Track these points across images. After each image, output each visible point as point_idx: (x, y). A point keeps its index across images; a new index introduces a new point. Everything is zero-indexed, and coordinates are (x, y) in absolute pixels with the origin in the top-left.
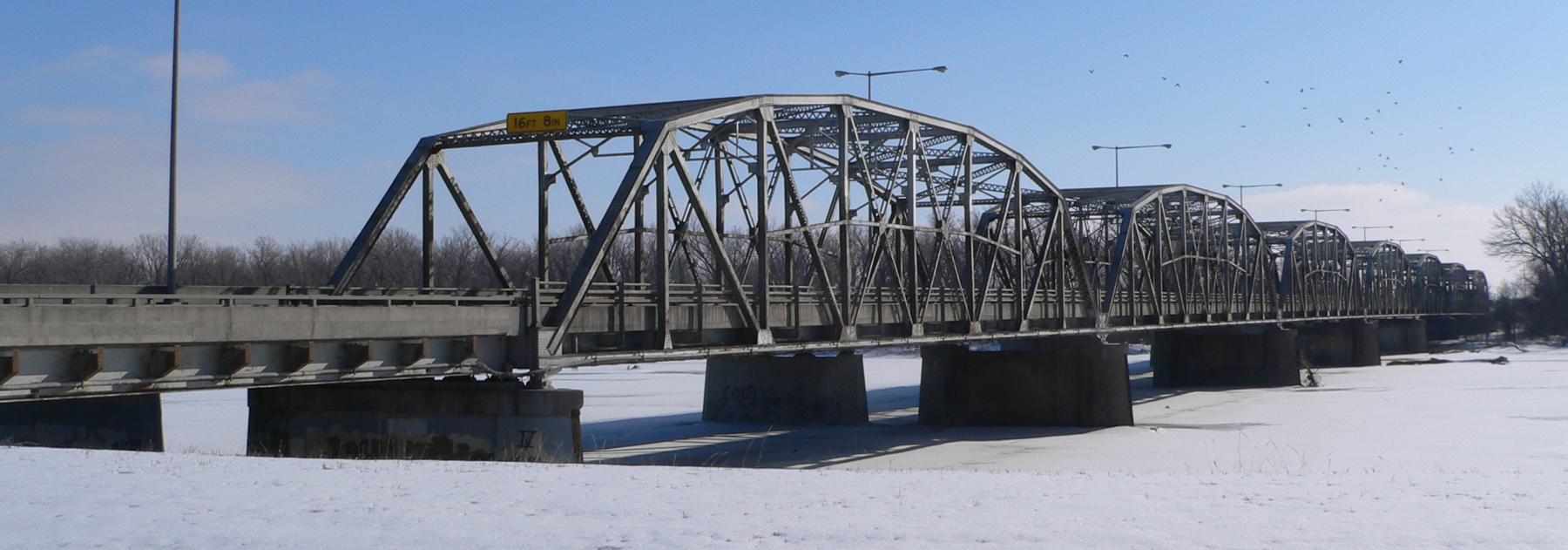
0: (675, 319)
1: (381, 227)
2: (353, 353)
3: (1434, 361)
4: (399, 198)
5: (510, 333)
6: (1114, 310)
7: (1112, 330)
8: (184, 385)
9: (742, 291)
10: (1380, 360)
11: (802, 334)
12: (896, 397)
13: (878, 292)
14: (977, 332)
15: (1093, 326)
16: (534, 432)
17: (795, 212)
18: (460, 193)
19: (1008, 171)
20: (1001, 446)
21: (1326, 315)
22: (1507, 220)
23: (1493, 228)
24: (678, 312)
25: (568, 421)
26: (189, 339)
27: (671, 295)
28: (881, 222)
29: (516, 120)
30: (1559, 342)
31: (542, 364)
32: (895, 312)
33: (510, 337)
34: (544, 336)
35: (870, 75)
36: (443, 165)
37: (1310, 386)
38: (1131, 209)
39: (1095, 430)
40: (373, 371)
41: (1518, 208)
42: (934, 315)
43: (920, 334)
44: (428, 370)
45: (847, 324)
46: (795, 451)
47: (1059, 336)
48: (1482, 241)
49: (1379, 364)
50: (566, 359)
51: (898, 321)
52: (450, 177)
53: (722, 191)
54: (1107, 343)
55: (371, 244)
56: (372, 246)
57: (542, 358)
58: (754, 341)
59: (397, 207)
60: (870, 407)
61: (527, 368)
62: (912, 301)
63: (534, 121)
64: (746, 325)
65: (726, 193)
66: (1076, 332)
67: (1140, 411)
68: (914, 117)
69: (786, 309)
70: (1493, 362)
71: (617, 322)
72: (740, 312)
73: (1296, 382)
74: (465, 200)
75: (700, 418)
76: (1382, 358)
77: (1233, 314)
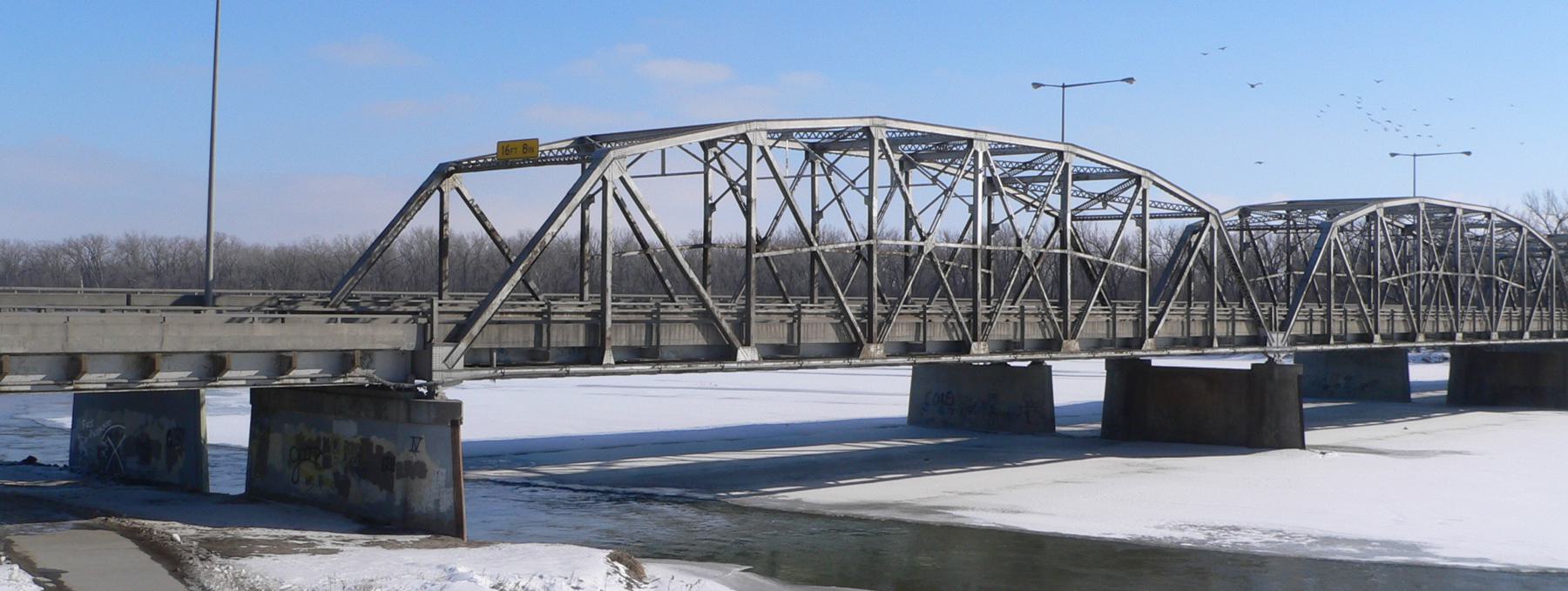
0: (1220, 330)
1: (386, 244)
2: (346, 361)
4: (408, 218)
6: (1297, 328)
7: (1294, 348)
8: (29, 388)
9: (716, 310)
11: (1349, 338)
12: (1078, 412)
13: (1222, 300)
16: (421, 439)
17: (914, 227)
24: (630, 330)
25: (447, 430)
27: (440, 313)
28: (926, 241)
31: (436, 377)
32: (1043, 325)
34: (439, 352)
35: (1064, 86)
40: (247, 380)
43: (982, 352)
44: (312, 379)
47: (1371, 349)
50: (469, 372)
51: (1048, 337)
55: (374, 260)
56: (375, 262)
61: (424, 380)
62: (1416, 309)
63: (516, 149)
66: (956, 359)
67: (1311, 437)
68: (979, 136)
69: (644, 331)
71: (545, 338)
75: (905, 422)
77: (1557, 332)
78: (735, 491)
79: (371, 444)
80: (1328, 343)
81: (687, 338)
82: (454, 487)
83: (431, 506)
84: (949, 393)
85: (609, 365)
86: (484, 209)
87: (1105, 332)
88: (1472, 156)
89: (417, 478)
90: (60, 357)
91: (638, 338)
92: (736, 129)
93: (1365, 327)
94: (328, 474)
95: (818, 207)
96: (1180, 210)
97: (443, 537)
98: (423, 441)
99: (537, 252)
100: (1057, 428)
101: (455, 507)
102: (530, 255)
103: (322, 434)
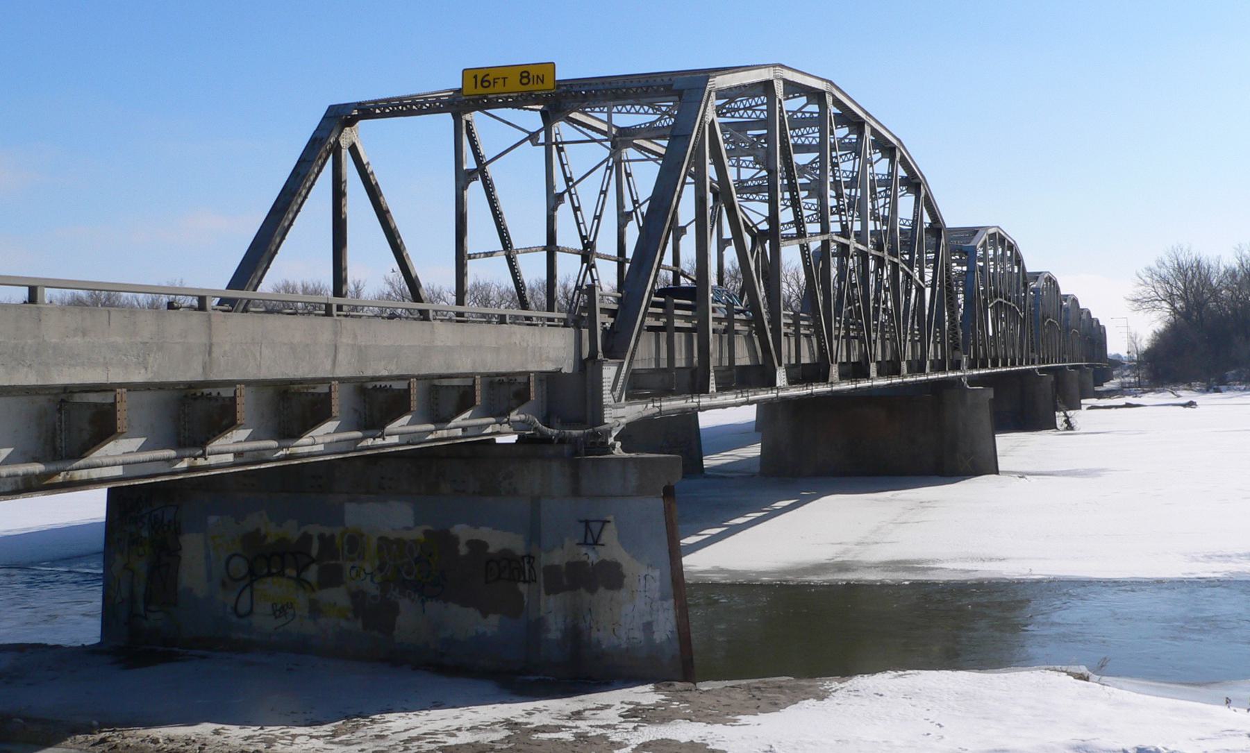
3: (1128, 405)
10: (1081, 404)
16: (605, 522)
18: (377, 184)
21: (897, 372)
22: (1148, 280)
23: (1135, 287)
26: (138, 377)
29: (476, 77)
30: (1204, 389)
36: (357, 145)
37: (1067, 429)
39: (964, 479)
41: (1157, 269)
48: (1124, 298)
49: (1080, 408)
52: (365, 163)
53: (624, 207)
54: (968, 387)
59: (305, 197)
70: (1184, 405)
73: (1051, 425)
74: (381, 195)
76: (1083, 401)
79: (455, 540)
80: (867, 376)
83: (638, 635)
89: (601, 590)
90: (147, 396)
93: (1003, 352)
94: (337, 596)
101: (678, 630)
103: (314, 530)
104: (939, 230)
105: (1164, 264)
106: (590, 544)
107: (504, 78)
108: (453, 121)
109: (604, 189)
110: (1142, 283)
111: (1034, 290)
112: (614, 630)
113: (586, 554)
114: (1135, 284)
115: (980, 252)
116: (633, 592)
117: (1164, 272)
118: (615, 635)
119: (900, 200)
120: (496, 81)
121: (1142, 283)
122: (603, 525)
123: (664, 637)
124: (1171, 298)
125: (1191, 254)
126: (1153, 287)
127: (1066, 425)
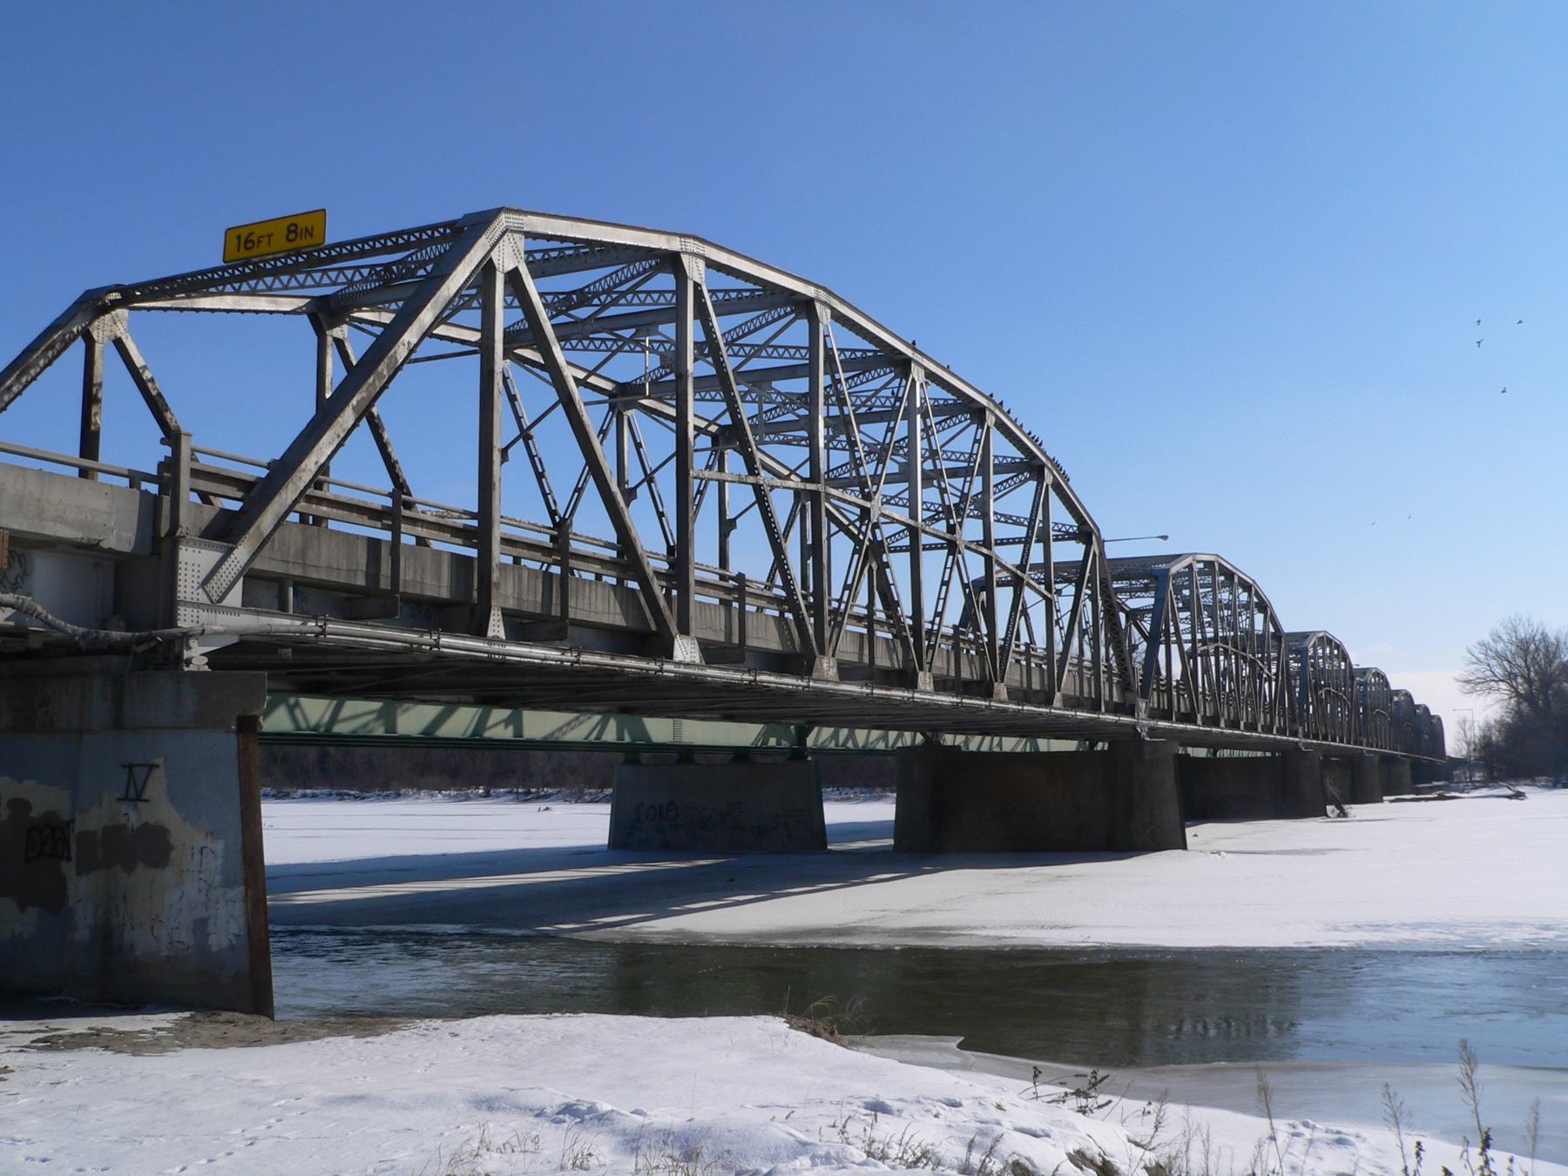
5: (110, 542)
7: (1152, 723)
14: (1002, 698)
15: (1133, 715)
16: (152, 767)
19: (1033, 484)
20: (1022, 874)
22: (1482, 657)
23: (1467, 665)
33: (110, 551)
34: (194, 561)
37: (1339, 816)
38: (1168, 570)
39: (1138, 855)
42: (945, 666)
45: (823, 652)
46: (732, 880)
48: (1454, 679)
54: (1148, 739)
57: (186, 603)
58: (669, 655)
60: (829, 839)
64: (653, 627)
65: (631, 485)
72: (643, 600)
75: (606, 848)
78: (1423, 783)
81: (600, 609)
82: (247, 885)
83: (186, 937)
84: (671, 803)
85: (496, 640)
86: (162, 386)
87: (1017, 677)
88: (1169, 539)
91: (531, 598)
92: (669, 241)
95: (627, 483)
96: (1060, 530)
97: (226, 1015)
98: (159, 774)
99: (381, 376)
100: (829, 847)
101: (249, 933)
102: (371, 380)
104: (1281, 637)
105: (1499, 637)
106: (130, 800)
107: (269, 236)
108: (316, 338)
109: (939, 610)
110: (1475, 660)
111: (1396, 703)
112: (152, 929)
113: (126, 814)
114: (1466, 662)
115: (1311, 653)
116: (183, 871)
117: (1500, 647)
118: (155, 937)
119: (1255, 616)
120: (261, 239)
121: (1475, 660)
122: (150, 771)
123: (225, 944)
124: (1510, 677)
125: (1532, 624)
126: (1489, 665)
127: (1338, 812)
